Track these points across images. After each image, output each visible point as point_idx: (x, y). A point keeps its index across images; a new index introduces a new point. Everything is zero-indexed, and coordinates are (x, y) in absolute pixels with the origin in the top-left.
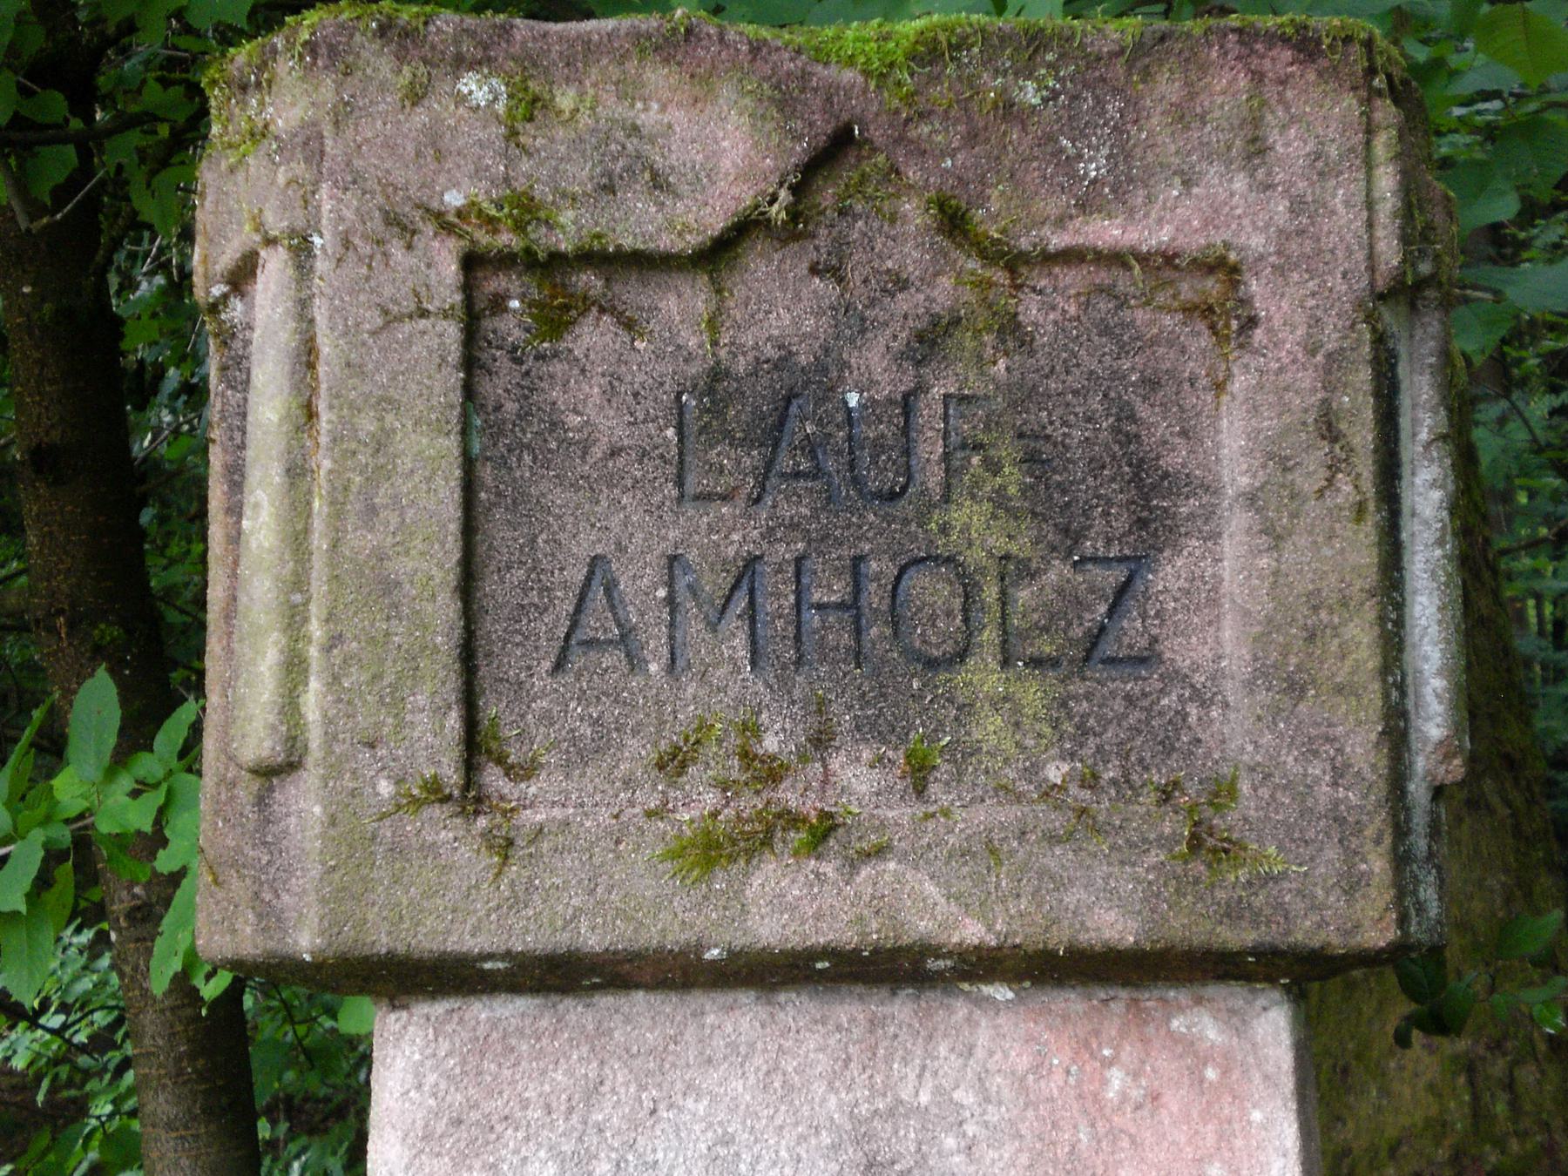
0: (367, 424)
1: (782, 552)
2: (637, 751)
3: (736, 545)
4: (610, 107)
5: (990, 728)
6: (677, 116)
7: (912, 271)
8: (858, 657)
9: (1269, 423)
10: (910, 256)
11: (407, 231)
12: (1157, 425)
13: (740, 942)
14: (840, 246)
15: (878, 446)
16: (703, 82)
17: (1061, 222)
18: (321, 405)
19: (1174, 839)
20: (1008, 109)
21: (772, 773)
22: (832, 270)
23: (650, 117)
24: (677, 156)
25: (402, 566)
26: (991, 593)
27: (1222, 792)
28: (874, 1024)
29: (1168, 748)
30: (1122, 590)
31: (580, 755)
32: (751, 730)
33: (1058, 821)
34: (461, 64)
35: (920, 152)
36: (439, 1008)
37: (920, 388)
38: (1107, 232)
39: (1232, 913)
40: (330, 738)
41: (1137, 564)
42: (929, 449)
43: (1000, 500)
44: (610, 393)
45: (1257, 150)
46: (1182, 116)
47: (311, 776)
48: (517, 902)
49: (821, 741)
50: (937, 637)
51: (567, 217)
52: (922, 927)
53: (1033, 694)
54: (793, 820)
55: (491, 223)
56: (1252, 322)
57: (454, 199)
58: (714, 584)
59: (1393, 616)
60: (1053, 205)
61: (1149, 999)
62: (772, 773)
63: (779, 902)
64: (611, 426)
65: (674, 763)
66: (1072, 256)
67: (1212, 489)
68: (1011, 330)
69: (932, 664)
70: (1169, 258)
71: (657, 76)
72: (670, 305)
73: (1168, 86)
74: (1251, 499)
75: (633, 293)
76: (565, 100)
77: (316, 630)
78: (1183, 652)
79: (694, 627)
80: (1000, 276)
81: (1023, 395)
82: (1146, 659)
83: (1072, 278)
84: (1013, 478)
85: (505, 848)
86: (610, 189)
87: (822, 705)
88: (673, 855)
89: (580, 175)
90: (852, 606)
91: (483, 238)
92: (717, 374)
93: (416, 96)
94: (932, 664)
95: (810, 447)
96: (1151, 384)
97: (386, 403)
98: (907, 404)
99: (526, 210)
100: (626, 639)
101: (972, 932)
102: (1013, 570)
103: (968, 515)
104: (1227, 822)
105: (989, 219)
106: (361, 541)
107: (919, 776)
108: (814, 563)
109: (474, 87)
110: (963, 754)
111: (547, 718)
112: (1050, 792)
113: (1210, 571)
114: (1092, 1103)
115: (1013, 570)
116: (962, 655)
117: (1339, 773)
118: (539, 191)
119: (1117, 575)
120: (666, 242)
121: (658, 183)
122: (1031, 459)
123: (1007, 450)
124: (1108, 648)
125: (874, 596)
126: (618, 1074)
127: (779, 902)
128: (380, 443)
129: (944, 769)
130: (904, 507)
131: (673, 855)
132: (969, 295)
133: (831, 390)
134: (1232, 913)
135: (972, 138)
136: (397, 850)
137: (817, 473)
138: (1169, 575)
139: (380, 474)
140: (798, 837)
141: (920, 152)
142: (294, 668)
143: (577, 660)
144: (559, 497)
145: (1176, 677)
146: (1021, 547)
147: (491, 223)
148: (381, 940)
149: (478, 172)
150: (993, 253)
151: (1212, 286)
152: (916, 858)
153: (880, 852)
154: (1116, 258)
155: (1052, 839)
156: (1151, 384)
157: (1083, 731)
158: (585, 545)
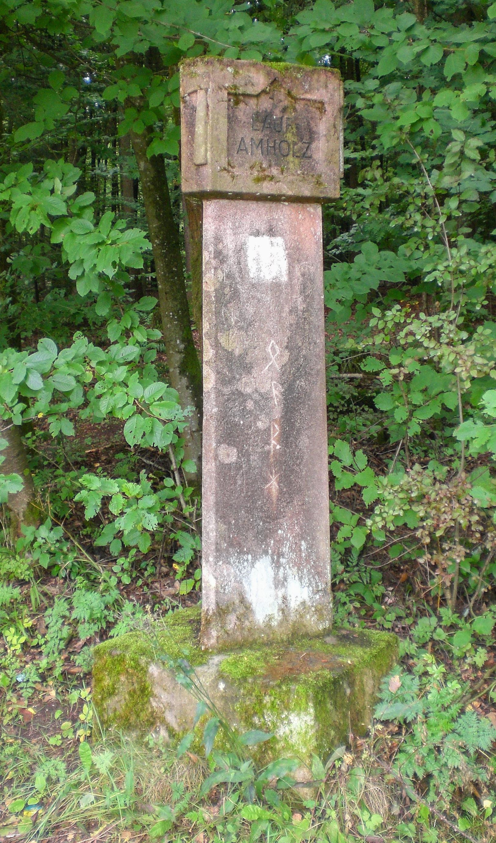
0: (216, 117)
1: (266, 139)
2: (247, 166)
3: (260, 137)
4: (247, 73)
5: (291, 165)
6: (255, 75)
7: (283, 100)
8: (275, 154)
9: (327, 125)
10: (282, 97)
11: (220, 89)
12: (313, 124)
13: (262, 192)
14: (273, 95)
15: (278, 124)
16: (258, 71)
17: (303, 94)
18: (209, 113)
19: (314, 182)
20: (296, 78)
21: (264, 170)
22: (272, 98)
23: (251, 75)
24: (255, 81)
25: (220, 137)
26: (292, 146)
27: (320, 176)
28: (271, 207)
29: (312, 169)
30: (308, 147)
31: (241, 165)
32: (261, 164)
33: (301, 179)
34: (228, 66)
35: (285, 83)
36: (216, 201)
37: (283, 117)
38: (308, 96)
39: (321, 192)
40: (212, 160)
41: (310, 143)
42: (284, 125)
43: (293, 133)
44: (244, 114)
45: (326, 86)
46: (318, 81)
47: (208, 166)
48: (235, 185)
49: (270, 166)
50: (285, 152)
51: (241, 88)
52: (284, 192)
53: (297, 161)
54: (269, 176)
55: (231, 89)
56: (325, 111)
57: (227, 85)
58: (257, 142)
59: (39, 32)
60: (302, 92)
61: (305, 205)
62: (264, 170)
63: (267, 187)
64: (244, 119)
65: (252, 168)
66: (304, 99)
67: (319, 134)
68: (295, 109)
69: (284, 156)
70: (315, 101)
71: (252, 69)
72: (252, 102)
73: (316, 76)
74: (325, 136)
75: (247, 100)
76: (241, 72)
77: (209, 145)
78: (315, 156)
79: (255, 149)
80: (293, 101)
81: (296, 118)
82: (310, 157)
83: (302, 102)
84: (295, 130)
85: (233, 177)
86: (246, 85)
87: (270, 161)
88: (254, 180)
89: (243, 83)
90: (274, 147)
91: (230, 90)
92: (258, 112)
93: (222, 70)
94: (284, 156)
95: (269, 124)
96: (312, 118)
97: (218, 114)
98: (282, 118)
99: (235, 87)
100: (246, 150)
101: (290, 193)
102: (295, 144)
103: (289, 135)
104: (321, 180)
105: (294, 93)
106: (215, 133)
107: (282, 172)
108: (270, 140)
109: (230, 69)
110: (288, 169)
111: (236, 160)
112: (298, 175)
113: (391, 174)
114: (297, 219)
115: (295, 144)
116: (287, 155)
117: (334, 174)
118: (238, 85)
119: (307, 145)
120: (253, 93)
121: (253, 85)
122: (297, 128)
123: (294, 126)
124: (306, 155)
125: (277, 146)
126: (239, 212)
127: (267, 187)
128: (217, 119)
129: (285, 171)
130: (281, 133)
131: (254, 180)
132: (289, 103)
133: (272, 116)
134: (321, 192)
135: (292, 82)
136: (220, 177)
137: (270, 127)
138: (313, 146)
139: (218, 123)
140: (269, 179)
141: (285, 83)
142: (206, 150)
143: (240, 152)
144: (237, 128)
145: (314, 160)
146: (295, 140)
147: (231, 89)
148: (219, 189)
149: (230, 81)
150: (292, 97)
151: (320, 105)
152: (283, 182)
153: (279, 181)
154: (309, 100)
155: (300, 181)
156: (312, 118)
157: (302, 167)
158: (241, 136)
